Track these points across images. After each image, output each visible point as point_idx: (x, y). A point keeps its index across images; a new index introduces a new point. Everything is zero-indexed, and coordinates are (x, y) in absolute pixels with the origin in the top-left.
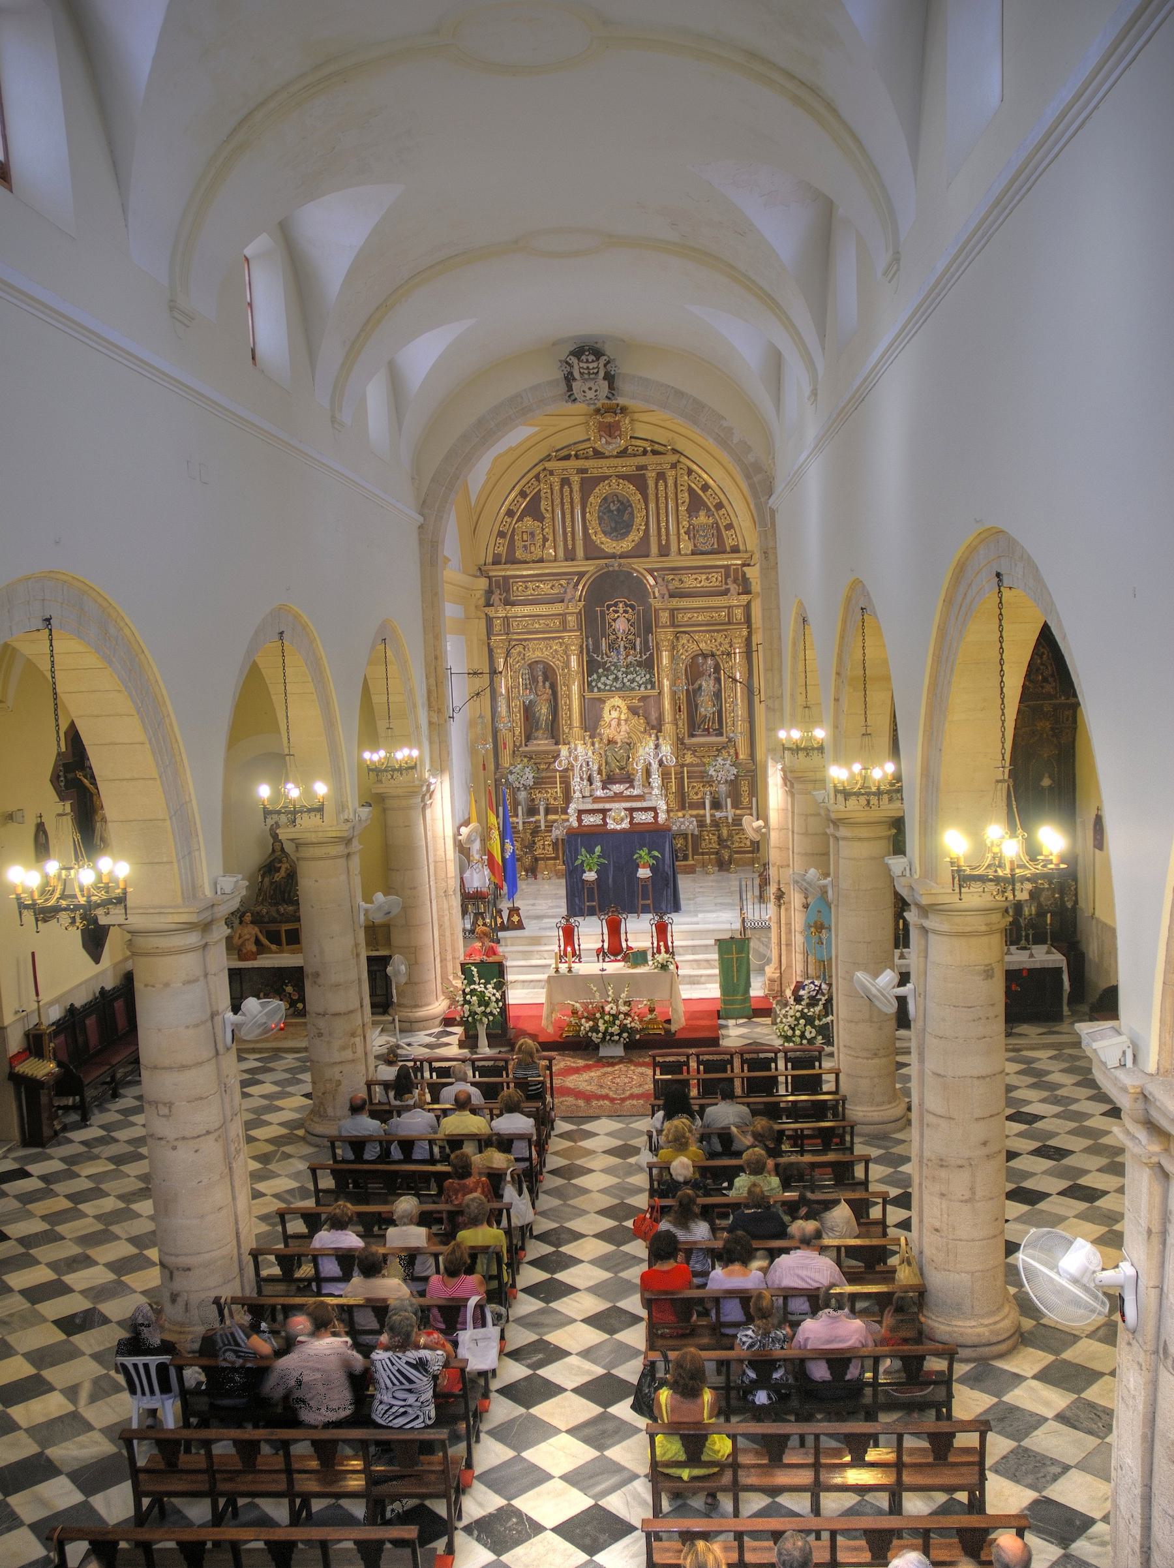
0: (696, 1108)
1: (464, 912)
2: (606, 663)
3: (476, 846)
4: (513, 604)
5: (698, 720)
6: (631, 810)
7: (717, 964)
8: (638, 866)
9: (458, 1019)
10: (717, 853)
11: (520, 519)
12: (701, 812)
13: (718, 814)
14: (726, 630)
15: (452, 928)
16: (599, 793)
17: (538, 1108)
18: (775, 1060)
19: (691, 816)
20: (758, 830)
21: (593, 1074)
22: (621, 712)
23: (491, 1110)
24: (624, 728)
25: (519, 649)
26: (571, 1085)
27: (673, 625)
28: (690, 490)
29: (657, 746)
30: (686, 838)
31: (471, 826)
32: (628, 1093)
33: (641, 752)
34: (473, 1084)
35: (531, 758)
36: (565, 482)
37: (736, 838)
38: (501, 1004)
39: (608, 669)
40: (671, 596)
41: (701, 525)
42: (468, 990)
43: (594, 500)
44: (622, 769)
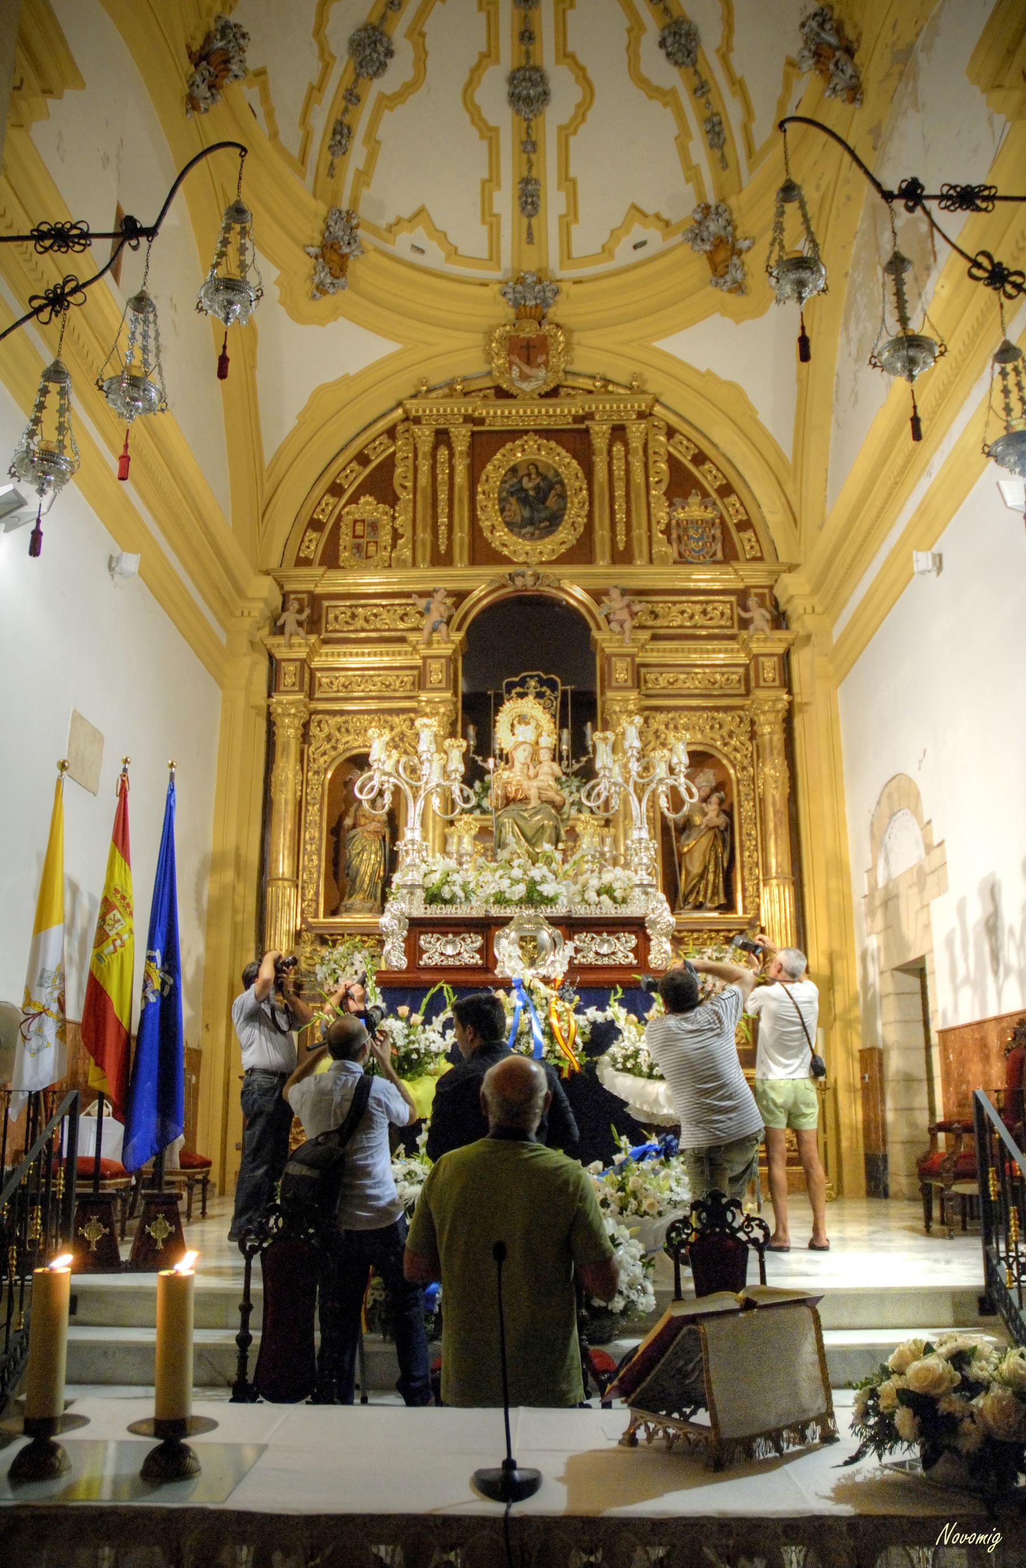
11: (354, 499)
28: (672, 460)
36: (442, 437)
41: (694, 522)
43: (494, 472)
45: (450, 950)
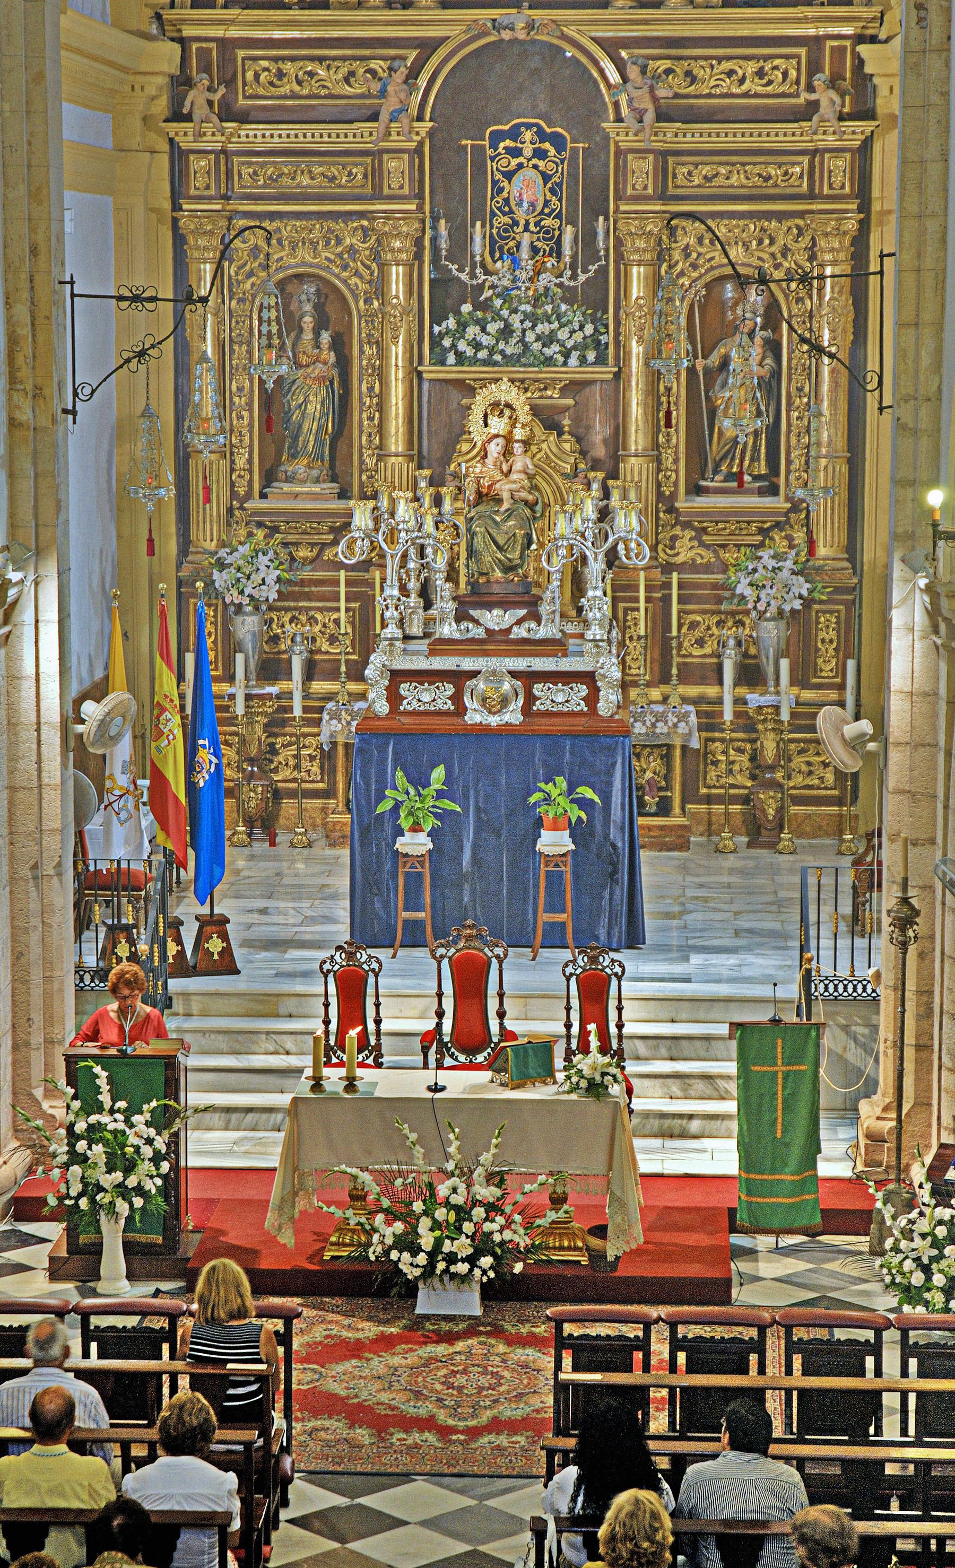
0: (663, 1463)
1: (82, 923)
2: (480, 288)
3: (123, 751)
4: (243, 118)
5: (714, 450)
6: (529, 678)
7: (733, 1087)
8: (539, 823)
9: (52, 1201)
10: (746, 800)
12: (711, 691)
13: (754, 699)
14: (801, 214)
15: (47, 963)
16: (448, 630)
17: (248, 1445)
18: (876, 1349)
19: (685, 700)
20: (855, 744)
21: (396, 1361)
22: (513, 422)
23: (125, 1446)
24: (520, 461)
25: (256, 239)
26: (339, 1390)
27: (663, 196)
29: (604, 514)
30: (667, 758)
31: (111, 700)
32: (486, 1416)
33: (562, 526)
34: (81, 1374)
35: (275, 530)
37: (798, 762)
38: (165, 1166)
39: (485, 306)
40: (661, 116)
42: (80, 1127)
44: (508, 569)
45: (426, 697)
